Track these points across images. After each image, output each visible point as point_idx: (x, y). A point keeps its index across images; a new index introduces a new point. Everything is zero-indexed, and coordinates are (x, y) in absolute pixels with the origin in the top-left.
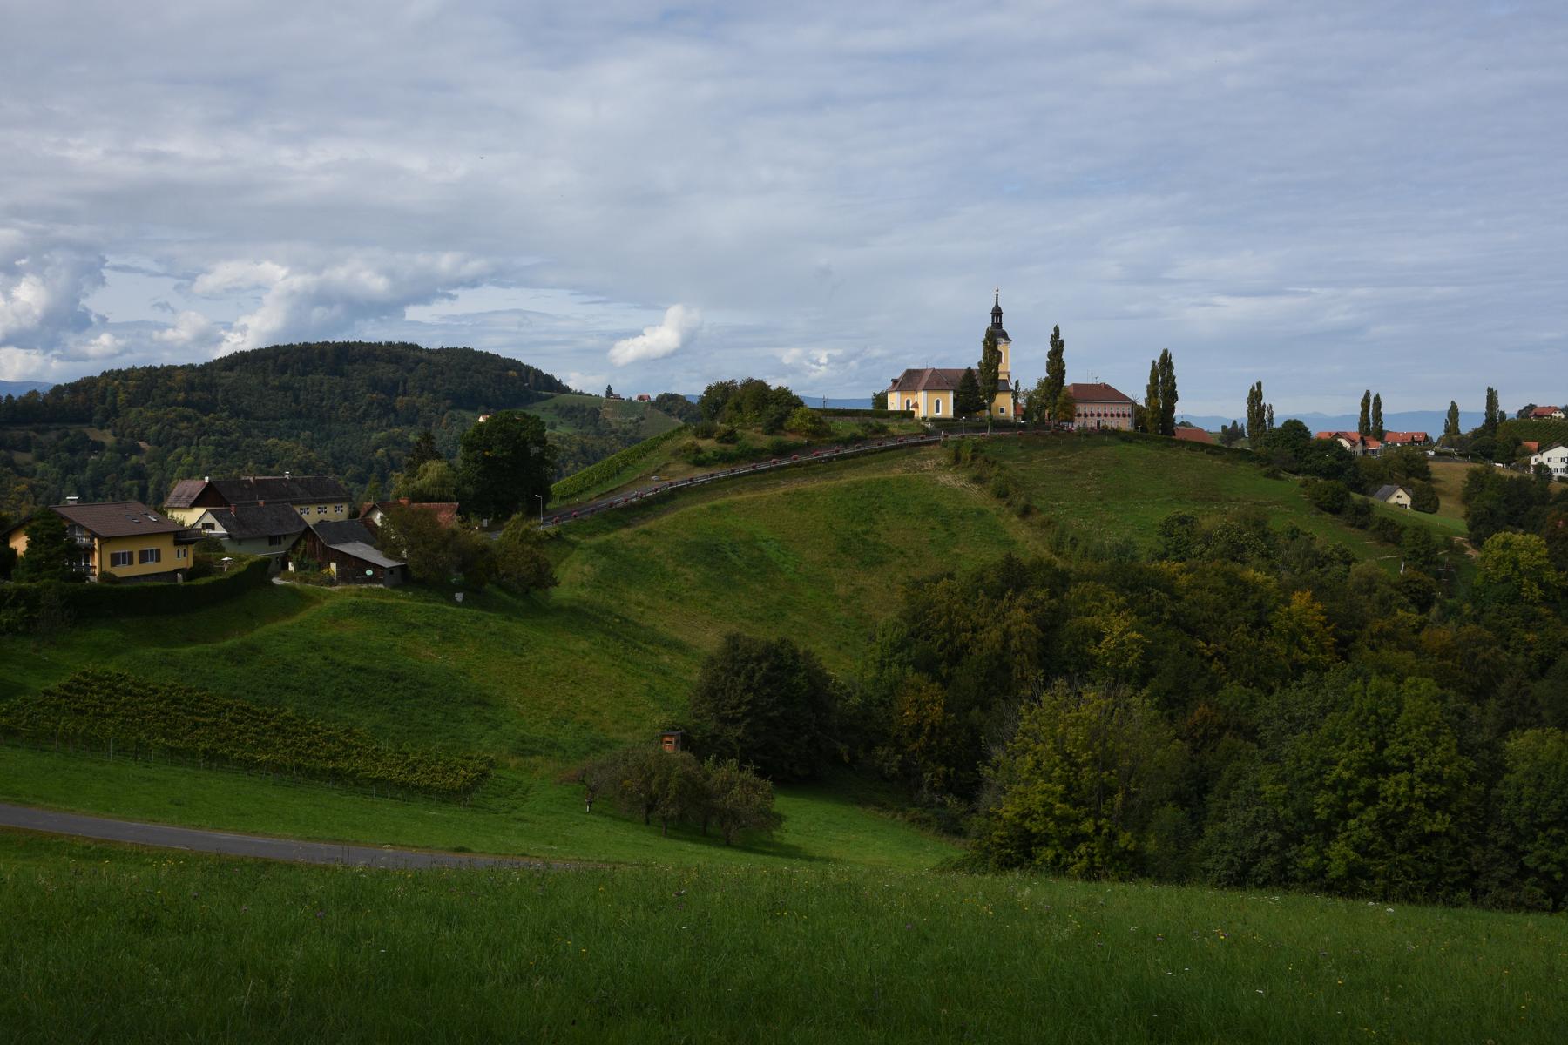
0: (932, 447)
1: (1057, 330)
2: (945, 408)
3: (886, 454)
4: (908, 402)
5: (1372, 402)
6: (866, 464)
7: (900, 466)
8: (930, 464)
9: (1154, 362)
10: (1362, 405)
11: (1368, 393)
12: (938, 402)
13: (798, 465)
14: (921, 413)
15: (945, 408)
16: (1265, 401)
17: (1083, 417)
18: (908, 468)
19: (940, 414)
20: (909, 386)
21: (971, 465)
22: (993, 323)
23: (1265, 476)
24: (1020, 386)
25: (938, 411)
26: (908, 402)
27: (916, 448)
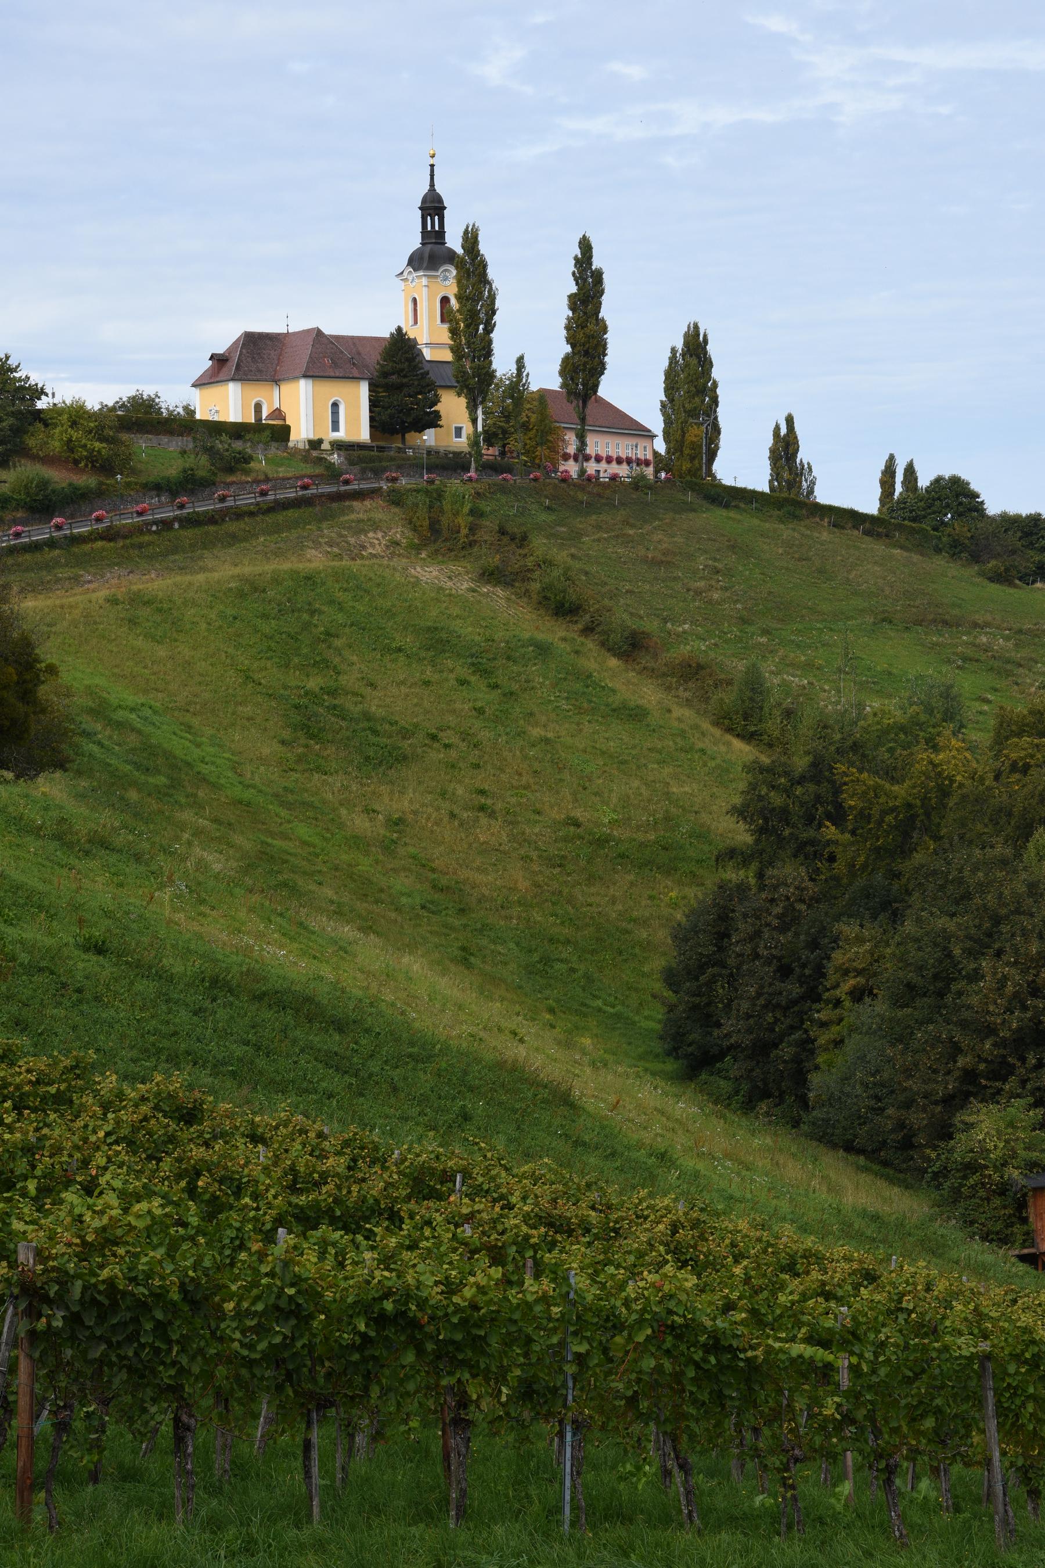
0: (368, 503)
1: (585, 246)
2: (353, 420)
3: (280, 517)
4: (258, 407)
5: (899, 477)
6: (245, 539)
7: (317, 545)
8: (376, 542)
9: (674, 350)
10: (883, 483)
11: (892, 458)
12: (335, 405)
13: (110, 535)
14: (301, 432)
15: (353, 420)
16: (804, 455)
17: (614, 462)
18: (336, 550)
19: (341, 435)
20: (260, 371)
21: (471, 544)
22: (424, 232)
23: (991, 580)
24: (529, 368)
25: (335, 427)
26: (258, 407)
27: (335, 505)
